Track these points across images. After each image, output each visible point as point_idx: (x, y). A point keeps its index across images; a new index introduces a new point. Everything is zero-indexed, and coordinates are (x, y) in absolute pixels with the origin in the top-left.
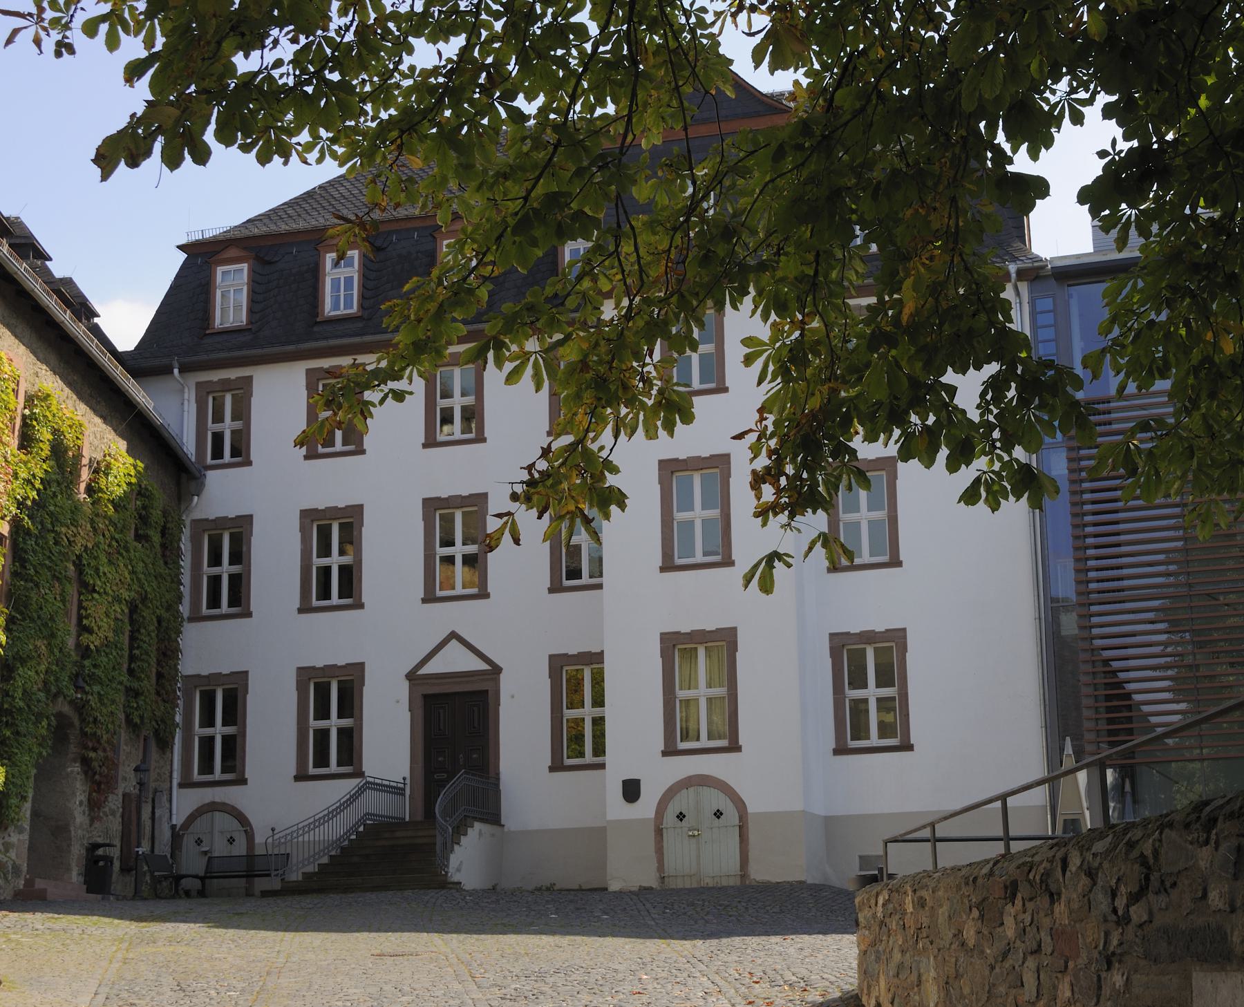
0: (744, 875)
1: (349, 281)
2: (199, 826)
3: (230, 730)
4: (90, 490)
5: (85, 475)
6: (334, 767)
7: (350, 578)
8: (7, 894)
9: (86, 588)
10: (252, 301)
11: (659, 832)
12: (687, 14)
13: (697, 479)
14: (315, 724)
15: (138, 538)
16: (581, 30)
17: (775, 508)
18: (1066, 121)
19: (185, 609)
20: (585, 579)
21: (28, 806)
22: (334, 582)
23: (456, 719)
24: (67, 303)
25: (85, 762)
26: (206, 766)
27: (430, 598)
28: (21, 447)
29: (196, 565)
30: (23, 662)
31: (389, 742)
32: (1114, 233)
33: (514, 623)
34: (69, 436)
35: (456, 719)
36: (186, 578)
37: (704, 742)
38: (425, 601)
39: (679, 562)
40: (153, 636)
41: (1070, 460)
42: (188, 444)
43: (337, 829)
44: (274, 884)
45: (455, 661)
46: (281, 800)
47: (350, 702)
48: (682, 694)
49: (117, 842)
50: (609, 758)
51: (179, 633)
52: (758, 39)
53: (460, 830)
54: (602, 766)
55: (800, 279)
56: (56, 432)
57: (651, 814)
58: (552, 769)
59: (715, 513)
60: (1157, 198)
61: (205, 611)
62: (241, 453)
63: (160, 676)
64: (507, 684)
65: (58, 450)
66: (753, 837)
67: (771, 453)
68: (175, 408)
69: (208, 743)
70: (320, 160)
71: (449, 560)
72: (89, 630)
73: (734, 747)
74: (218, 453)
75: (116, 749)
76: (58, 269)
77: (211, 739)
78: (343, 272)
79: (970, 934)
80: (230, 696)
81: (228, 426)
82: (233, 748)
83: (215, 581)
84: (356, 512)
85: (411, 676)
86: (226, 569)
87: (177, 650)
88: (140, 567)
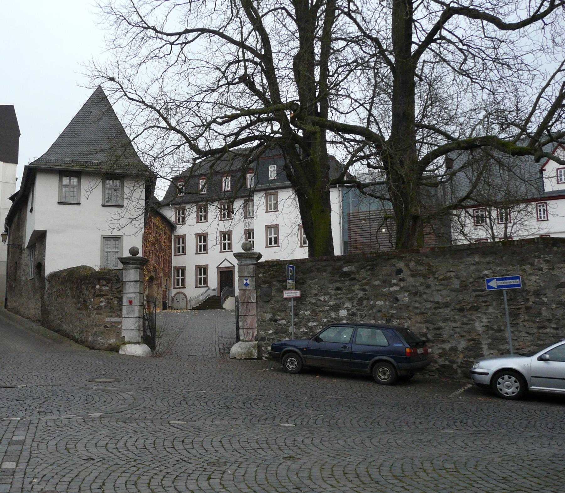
3: (205, 243)
13: (273, 229)
14: (199, 276)
22: (202, 248)
26: (178, 285)
43: (203, 298)
74: (179, 221)
77: (179, 279)
80: (182, 271)
85: (218, 268)
86: (181, 245)
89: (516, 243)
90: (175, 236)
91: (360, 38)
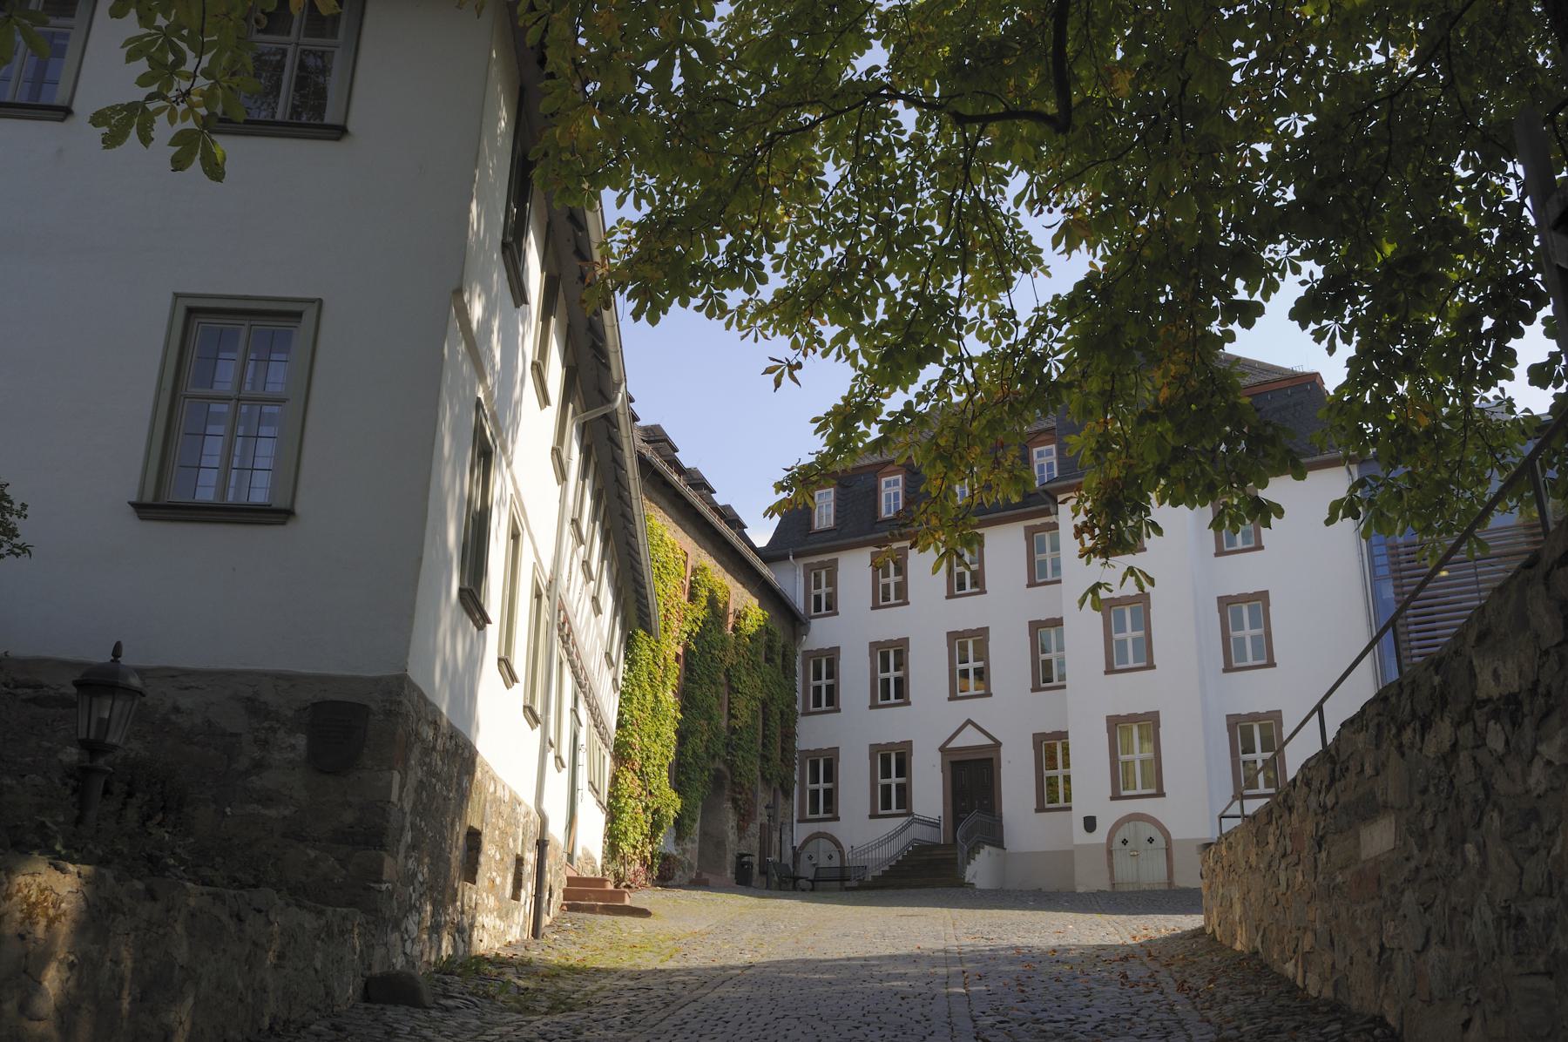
0: (1170, 883)
1: (896, 495)
2: (811, 846)
3: (828, 785)
4: (734, 629)
5: (731, 619)
6: (894, 810)
7: (901, 684)
8: (686, 881)
9: (733, 690)
10: (837, 511)
11: (1110, 853)
12: (1006, 218)
14: (881, 781)
15: (767, 660)
16: (930, 230)
17: (1092, 551)
18: (1289, 273)
19: (799, 707)
20: (1056, 682)
21: (697, 825)
22: (892, 689)
23: (972, 777)
24: (722, 516)
25: (734, 801)
26: (815, 810)
27: (953, 697)
28: (690, 600)
29: (806, 680)
30: (692, 734)
31: (929, 792)
32: (1325, 343)
33: (1009, 717)
34: (719, 594)
35: (972, 777)
36: (799, 687)
37: (1139, 791)
38: (950, 699)
39: (1117, 667)
40: (778, 724)
41: (1396, 587)
42: (800, 604)
44: (854, 883)
45: (971, 738)
46: (860, 830)
47: (903, 769)
48: (1123, 758)
49: (757, 855)
50: (1074, 803)
51: (795, 722)
52: (1055, 230)
53: (972, 852)
54: (1070, 809)
55: (1102, 393)
56: (711, 591)
57: (1104, 840)
58: (1037, 811)
59: (1141, 633)
60: (1352, 314)
61: (812, 709)
62: (832, 608)
63: (783, 750)
64: (1005, 754)
65: (712, 601)
66: (1176, 856)
67: (1087, 512)
68: (791, 581)
69: (815, 793)
70: (774, 334)
71: (965, 674)
72: (736, 717)
73: (1160, 794)
74: (818, 608)
75: (755, 795)
76: (720, 499)
78: (892, 490)
79: (1253, 859)
81: (823, 591)
82: (831, 796)
83: (818, 689)
84: (904, 642)
85: (942, 749)
86: (824, 682)
87: (794, 733)
88: (768, 678)
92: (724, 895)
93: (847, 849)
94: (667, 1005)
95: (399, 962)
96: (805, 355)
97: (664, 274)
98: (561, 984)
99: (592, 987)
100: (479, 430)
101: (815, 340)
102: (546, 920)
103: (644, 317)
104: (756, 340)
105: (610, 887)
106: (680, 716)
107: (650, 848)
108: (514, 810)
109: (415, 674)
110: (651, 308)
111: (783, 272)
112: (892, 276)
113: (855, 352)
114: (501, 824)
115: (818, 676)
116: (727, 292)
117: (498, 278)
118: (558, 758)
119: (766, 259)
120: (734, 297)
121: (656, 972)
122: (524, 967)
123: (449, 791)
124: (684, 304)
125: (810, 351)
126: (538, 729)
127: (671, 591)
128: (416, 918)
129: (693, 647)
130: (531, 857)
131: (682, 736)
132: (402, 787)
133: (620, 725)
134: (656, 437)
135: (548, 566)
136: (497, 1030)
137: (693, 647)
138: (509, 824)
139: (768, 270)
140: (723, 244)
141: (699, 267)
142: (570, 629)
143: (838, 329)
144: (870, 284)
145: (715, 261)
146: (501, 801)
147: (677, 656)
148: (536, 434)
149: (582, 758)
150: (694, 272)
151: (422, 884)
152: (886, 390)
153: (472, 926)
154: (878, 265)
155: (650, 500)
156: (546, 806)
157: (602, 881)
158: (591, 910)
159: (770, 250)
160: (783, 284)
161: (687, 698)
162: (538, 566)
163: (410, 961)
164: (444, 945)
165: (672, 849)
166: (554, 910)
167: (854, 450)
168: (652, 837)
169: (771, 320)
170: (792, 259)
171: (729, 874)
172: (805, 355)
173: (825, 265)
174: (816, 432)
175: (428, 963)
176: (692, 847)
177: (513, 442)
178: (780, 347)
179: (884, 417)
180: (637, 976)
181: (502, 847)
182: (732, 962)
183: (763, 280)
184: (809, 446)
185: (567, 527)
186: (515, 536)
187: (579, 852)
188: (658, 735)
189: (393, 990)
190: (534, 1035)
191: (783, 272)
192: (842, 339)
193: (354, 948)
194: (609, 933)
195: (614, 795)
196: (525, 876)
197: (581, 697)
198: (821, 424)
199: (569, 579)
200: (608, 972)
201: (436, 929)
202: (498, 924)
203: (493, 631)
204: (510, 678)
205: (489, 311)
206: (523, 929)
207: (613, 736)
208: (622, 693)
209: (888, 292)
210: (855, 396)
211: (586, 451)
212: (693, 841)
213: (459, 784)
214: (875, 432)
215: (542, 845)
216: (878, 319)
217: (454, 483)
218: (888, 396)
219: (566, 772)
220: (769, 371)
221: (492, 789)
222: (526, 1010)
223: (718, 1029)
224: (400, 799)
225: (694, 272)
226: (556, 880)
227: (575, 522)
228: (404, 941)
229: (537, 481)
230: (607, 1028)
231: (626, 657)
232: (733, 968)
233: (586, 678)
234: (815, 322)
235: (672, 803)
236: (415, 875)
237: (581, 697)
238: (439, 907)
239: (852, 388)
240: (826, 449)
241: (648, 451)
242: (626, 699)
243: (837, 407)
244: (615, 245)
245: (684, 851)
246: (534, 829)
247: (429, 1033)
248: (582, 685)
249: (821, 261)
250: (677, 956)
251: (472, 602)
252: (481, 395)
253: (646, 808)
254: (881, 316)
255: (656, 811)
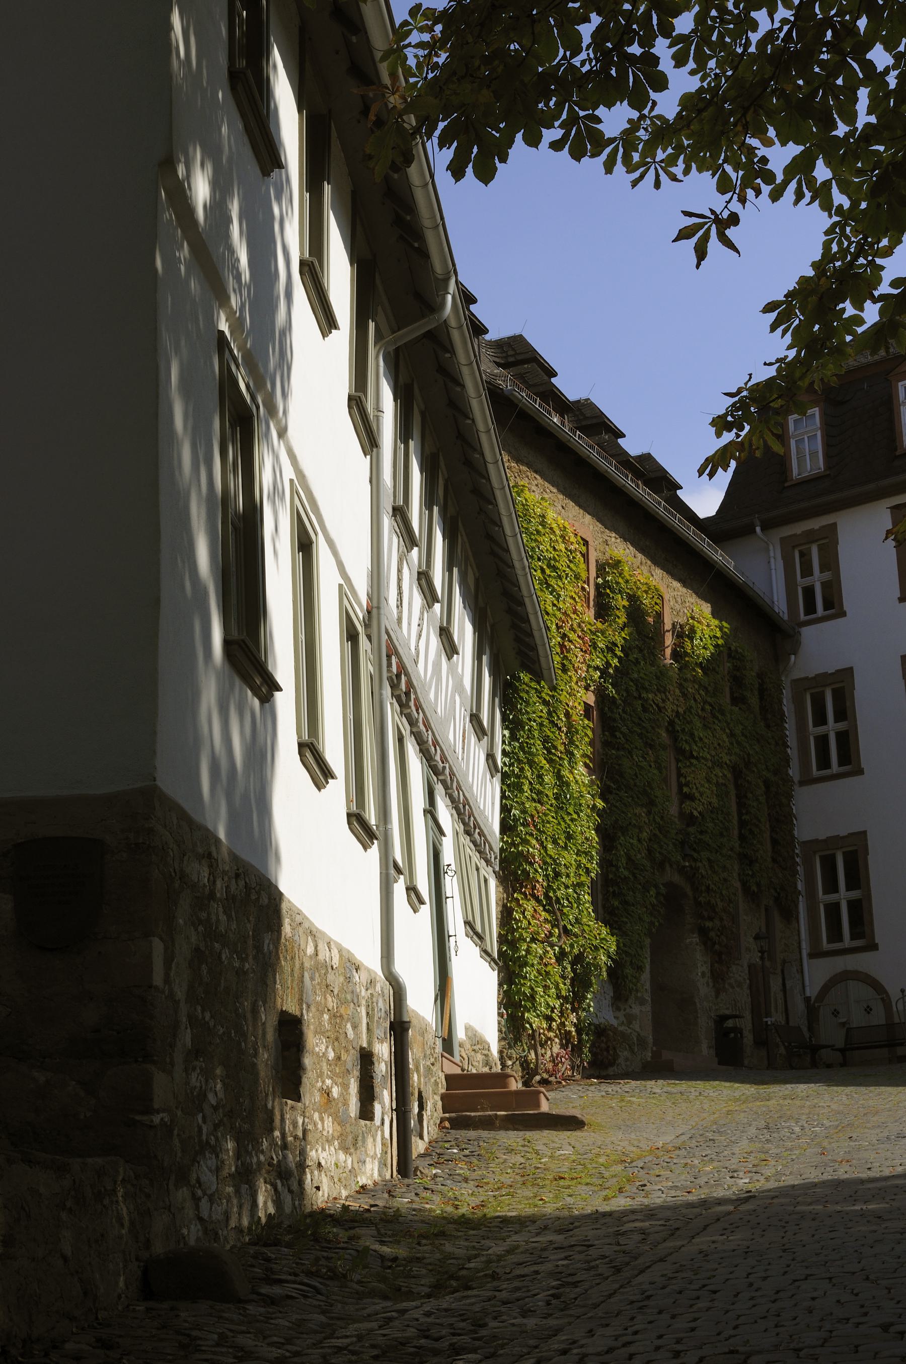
3: (855, 894)
4: (675, 655)
5: (669, 640)
9: (683, 755)
15: (735, 701)
19: (794, 772)
21: (646, 976)
24: (638, 475)
25: (703, 932)
26: (835, 934)
28: (598, 616)
40: (762, 798)
42: (779, 603)
49: (748, 1015)
51: (790, 797)
56: (633, 598)
61: (815, 772)
62: (834, 605)
63: (775, 842)
65: (636, 613)
68: (763, 569)
69: (833, 910)
70: (686, 172)
72: (691, 798)
74: (810, 608)
76: (632, 446)
81: (817, 578)
83: (822, 742)
86: (832, 727)
89: (235, 635)
90: (796, 682)
91: (721, 1122)
92: (700, 1084)
93: (894, 993)
94: (618, 1270)
95: (193, 1233)
96: (743, 200)
97: (500, 93)
98: (448, 1247)
99: (497, 1249)
100: (228, 383)
101: (757, 173)
102: (419, 1146)
103: (469, 170)
104: (657, 185)
105: (515, 1085)
106: (600, 804)
107: (573, 1018)
108: (349, 979)
109: (168, 783)
110: (481, 157)
111: (691, 65)
112: (879, 47)
113: (827, 184)
114: (331, 1002)
115: (820, 719)
116: (601, 112)
117: (228, 131)
118: (412, 890)
119: (662, 48)
120: (614, 119)
121: (598, 1217)
122: (388, 1223)
123: (243, 960)
124: (533, 141)
125: (750, 193)
126: (375, 850)
127: (566, 605)
128: (212, 1162)
129: (611, 691)
130: (383, 1050)
131: (608, 834)
132: (168, 960)
133: (506, 827)
134: (518, 355)
135: (362, 587)
136: (353, 1328)
137: (611, 691)
138: (343, 1002)
139: (666, 65)
140: (586, 31)
141: (551, 75)
142: (410, 684)
143: (794, 150)
144: (841, 67)
145: (576, 61)
146: (327, 967)
147: (587, 708)
148: (319, 369)
149: (451, 885)
150: (544, 85)
151: (215, 1108)
152: (885, 242)
153: (302, 1166)
154: (851, 29)
155: (518, 461)
156: (400, 968)
157: (502, 1078)
158: (488, 1124)
159: (666, 30)
160: (693, 84)
161: (606, 770)
162: (345, 591)
163: (210, 1230)
164: (261, 1200)
165: (609, 1017)
166: (430, 1129)
167: (840, 350)
168: (576, 1000)
169: (679, 149)
170: (705, 40)
171: (705, 1049)
172: (743, 200)
173: (762, 43)
174: (773, 328)
175: (239, 1230)
176: (641, 1011)
177: (285, 395)
178: (700, 191)
179: (884, 288)
180: (567, 1224)
181: (336, 1039)
182: (719, 1193)
183: (661, 83)
184: (764, 351)
185: (387, 522)
186: (304, 545)
187: (460, 1034)
188: (569, 837)
189: (187, 1277)
190: (411, 1332)
191: (691, 65)
192: (800, 167)
193: (120, 1220)
194: (519, 1159)
195: (509, 937)
196: (377, 1080)
197: (439, 789)
198: (781, 312)
199: (400, 605)
200: (521, 1223)
201: (245, 1177)
202: (344, 1160)
203: (286, 703)
204: (321, 773)
205: (220, 187)
206: (383, 1164)
207: (497, 845)
208: (505, 776)
209: (874, 77)
210: (834, 259)
211: (402, 395)
212: (642, 1002)
213: (258, 948)
214: (871, 313)
215: (399, 1028)
216: (860, 125)
217: (197, 472)
218: (888, 252)
219: (426, 911)
220: (684, 234)
221: (310, 950)
222: (400, 1294)
223: (701, 1305)
224: (167, 980)
225: (544, 85)
226: (429, 1082)
227: (400, 513)
228: (196, 1200)
229: (327, 451)
230: (525, 1313)
231: (504, 719)
232: (720, 1202)
233: (444, 759)
234: (754, 142)
235: (601, 942)
236: (203, 1096)
237: (439, 789)
238: (247, 1141)
239: (827, 245)
240: (792, 354)
241: (506, 382)
242: (511, 785)
243: (803, 280)
244: (410, 52)
245: (630, 1019)
246: (383, 1005)
247: (247, 1341)
248: (439, 771)
249: (754, 37)
250: (630, 1189)
251: (248, 663)
252: (224, 326)
253: (561, 957)
254: (864, 118)
255: (578, 959)
